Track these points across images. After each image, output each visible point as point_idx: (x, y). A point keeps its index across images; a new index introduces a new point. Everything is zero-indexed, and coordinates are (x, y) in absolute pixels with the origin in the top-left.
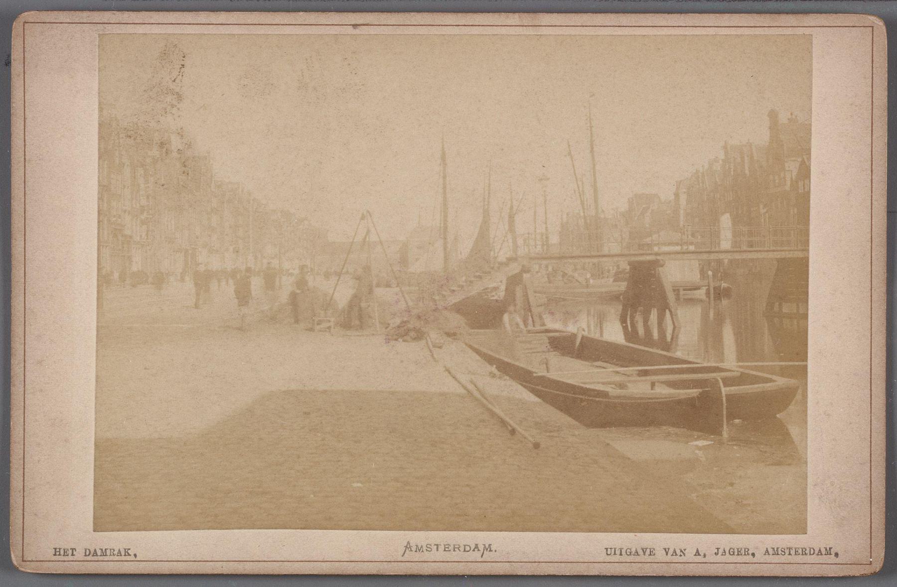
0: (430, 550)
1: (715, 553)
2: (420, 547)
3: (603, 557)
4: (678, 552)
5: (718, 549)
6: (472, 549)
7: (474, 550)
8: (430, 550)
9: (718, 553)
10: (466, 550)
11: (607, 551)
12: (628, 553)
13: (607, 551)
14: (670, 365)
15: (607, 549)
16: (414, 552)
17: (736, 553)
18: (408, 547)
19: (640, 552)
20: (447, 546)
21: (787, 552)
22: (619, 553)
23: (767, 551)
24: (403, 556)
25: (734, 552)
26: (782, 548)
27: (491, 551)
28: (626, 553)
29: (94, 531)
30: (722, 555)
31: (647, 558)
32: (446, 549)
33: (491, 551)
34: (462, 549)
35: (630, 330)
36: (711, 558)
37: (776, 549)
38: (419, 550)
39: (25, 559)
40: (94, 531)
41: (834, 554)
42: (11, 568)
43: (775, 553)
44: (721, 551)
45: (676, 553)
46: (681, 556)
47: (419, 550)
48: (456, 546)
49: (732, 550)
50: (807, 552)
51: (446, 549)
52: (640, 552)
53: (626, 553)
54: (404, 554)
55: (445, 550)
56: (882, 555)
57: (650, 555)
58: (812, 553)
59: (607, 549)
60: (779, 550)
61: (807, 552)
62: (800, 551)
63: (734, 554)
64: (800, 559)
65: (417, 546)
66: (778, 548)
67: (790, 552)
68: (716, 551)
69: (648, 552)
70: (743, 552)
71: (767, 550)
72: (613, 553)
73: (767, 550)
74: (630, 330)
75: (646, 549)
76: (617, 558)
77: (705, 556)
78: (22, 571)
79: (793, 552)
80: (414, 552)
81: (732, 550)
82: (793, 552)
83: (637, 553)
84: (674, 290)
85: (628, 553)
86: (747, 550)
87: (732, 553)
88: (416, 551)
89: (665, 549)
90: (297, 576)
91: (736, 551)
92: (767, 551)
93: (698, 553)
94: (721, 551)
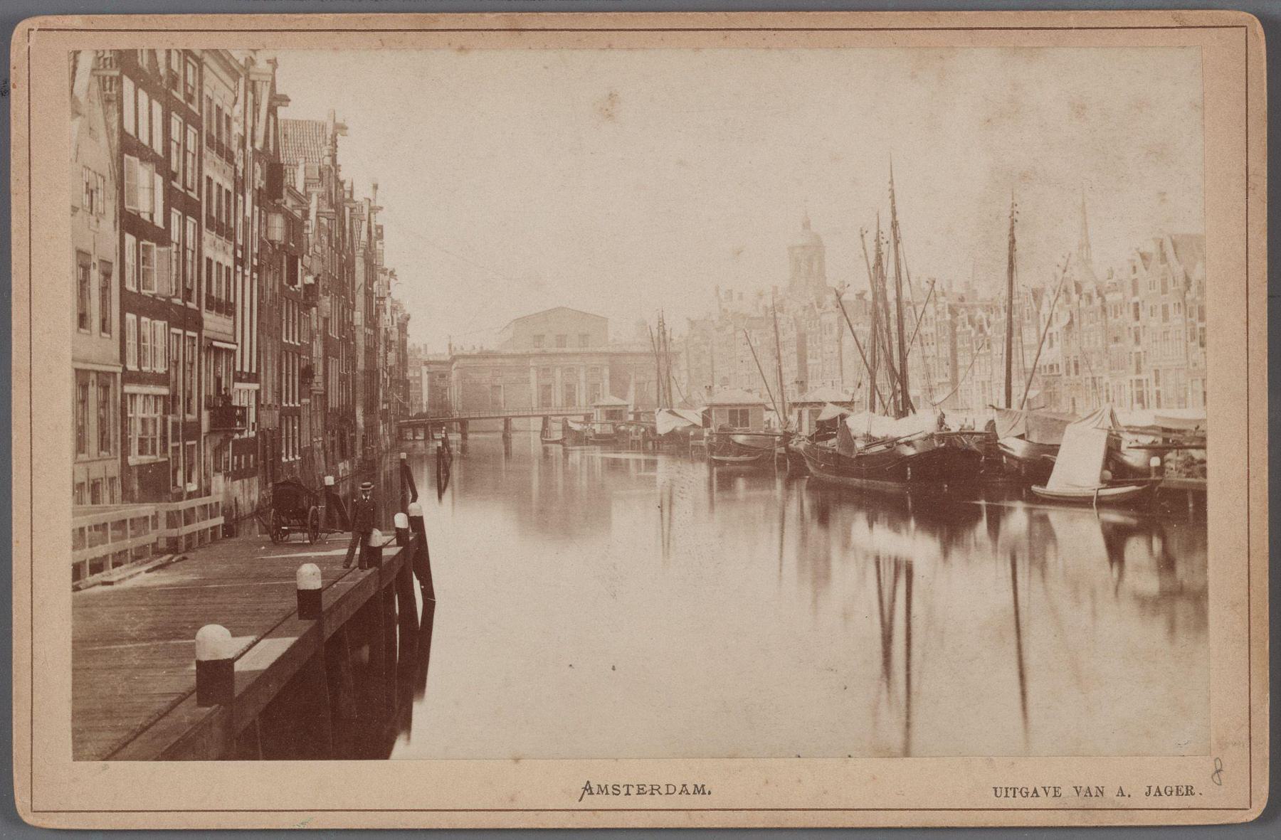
0: (618, 792)
2: (699, 787)
3: (993, 802)
4: (1093, 791)
5: (1150, 787)
8: (618, 792)
10: (670, 792)
11: (996, 791)
12: (1169, 793)
13: (996, 791)
16: (595, 795)
19: (1041, 792)
20: (641, 787)
24: (580, 800)
25: (1027, 793)
27: (704, 793)
30: (1155, 795)
32: (641, 791)
34: (663, 790)
35: (397, 612)
36: (1140, 800)
38: (699, 792)
42: (15, 819)
44: (1153, 790)
45: (1159, 792)
47: (699, 792)
51: (641, 791)
52: (1041, 792)
54: (581, 798)
55: (639, 794)
57: (1055, 796)
62: (1184, 790)
64: (635, 801)
65: (696, 786)
72: (1004, 794)
74: (397, 612)
76: (1030, 802)
78: (34, 828)
80: (611, 795)
82: (632, 791)
84: (1199, 597)
86: (1189, 788)
87: (1169, 793)
88: (694, 793)
90: (1052, 828)
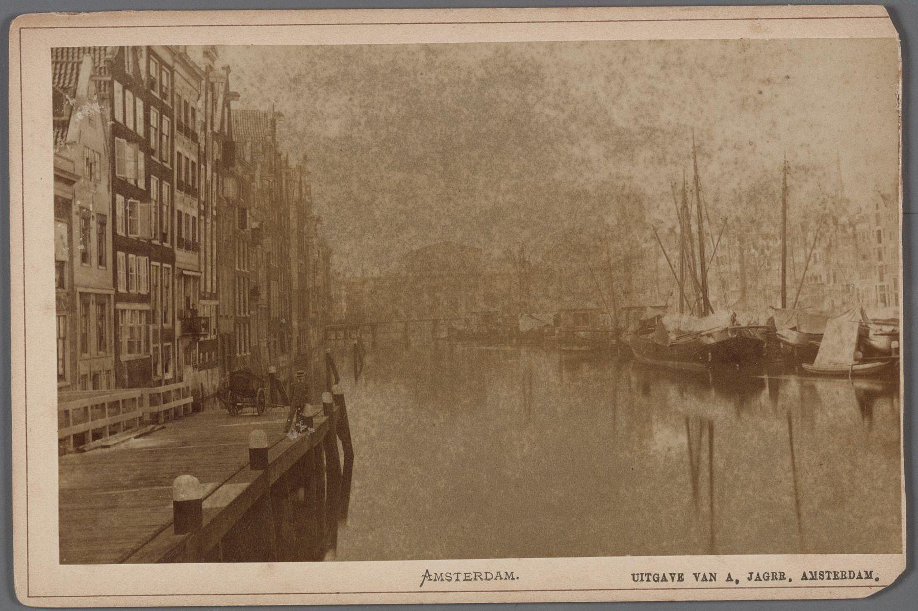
1: (748, 578)
5: (751, 574)
6: (494, 578)
7: (496, 579)
9: (751, 578)
12: (766, 578)
14: (429, 49)
15: (633, 575)
17: (771, 578)
18: (427, 575)
19: (668, 577)
20: (467, 575)
21: (826, 576)
22: (647, 579)
23: (804, 575)
24: (421, 586)
26: (821, 572)
27: (513, 579)
28: (764, 577)
29: (62, 562)
31: (676, 584)
33: (513, 579)
34: (483, 577)
37: (869, 573)
39: (30, 595)
40: (62, 562)
41: (735, 581)
43: (868, 576)
44: (754, 576)
45: (705, 578)
46: (711, 580)
48: (477, 574)
49: (766, 575)
50: (847, 575)
52: (668, 577)
53: (764, 577)
56: (358, 491)
58: (852, 576)
59: (633, 575)
60: (818, 574)
61: (847, 575)
63: (658, 581)
65: (436, 574)
66: (816, 572)
67: (648, 578)
68: (749, 576)
69: (676, 577)
70: (840, 575)
71: (804, 574)
72: (640, 579)
73: (804, 574)
75: (675, 574)
77: (790, 580)
79: (832, 576)
81: (766, 575)
83: (664, 579)
85: (656, 579)
89: (695, 574)
91: (771, 575)
92: (804, 575)
93: (729, 579)
94: (754, 576)
